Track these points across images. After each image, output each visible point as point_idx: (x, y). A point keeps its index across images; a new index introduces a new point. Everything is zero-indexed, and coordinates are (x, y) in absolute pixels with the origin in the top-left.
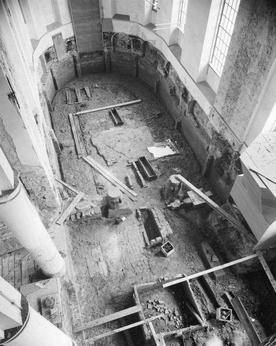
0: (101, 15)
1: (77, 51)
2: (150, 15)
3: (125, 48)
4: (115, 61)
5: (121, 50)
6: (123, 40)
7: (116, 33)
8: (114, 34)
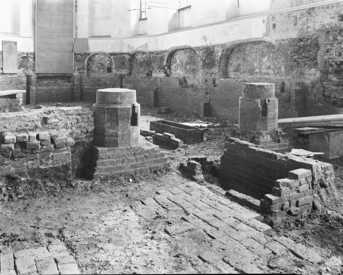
0: (74, 35)
1: (35, 71)
2: (137, 25)
3: (103, 72)
4: (88, 87)
5: (98, 75)
6: (101, 62)
7: (93, 54)
8: (90, 56)
